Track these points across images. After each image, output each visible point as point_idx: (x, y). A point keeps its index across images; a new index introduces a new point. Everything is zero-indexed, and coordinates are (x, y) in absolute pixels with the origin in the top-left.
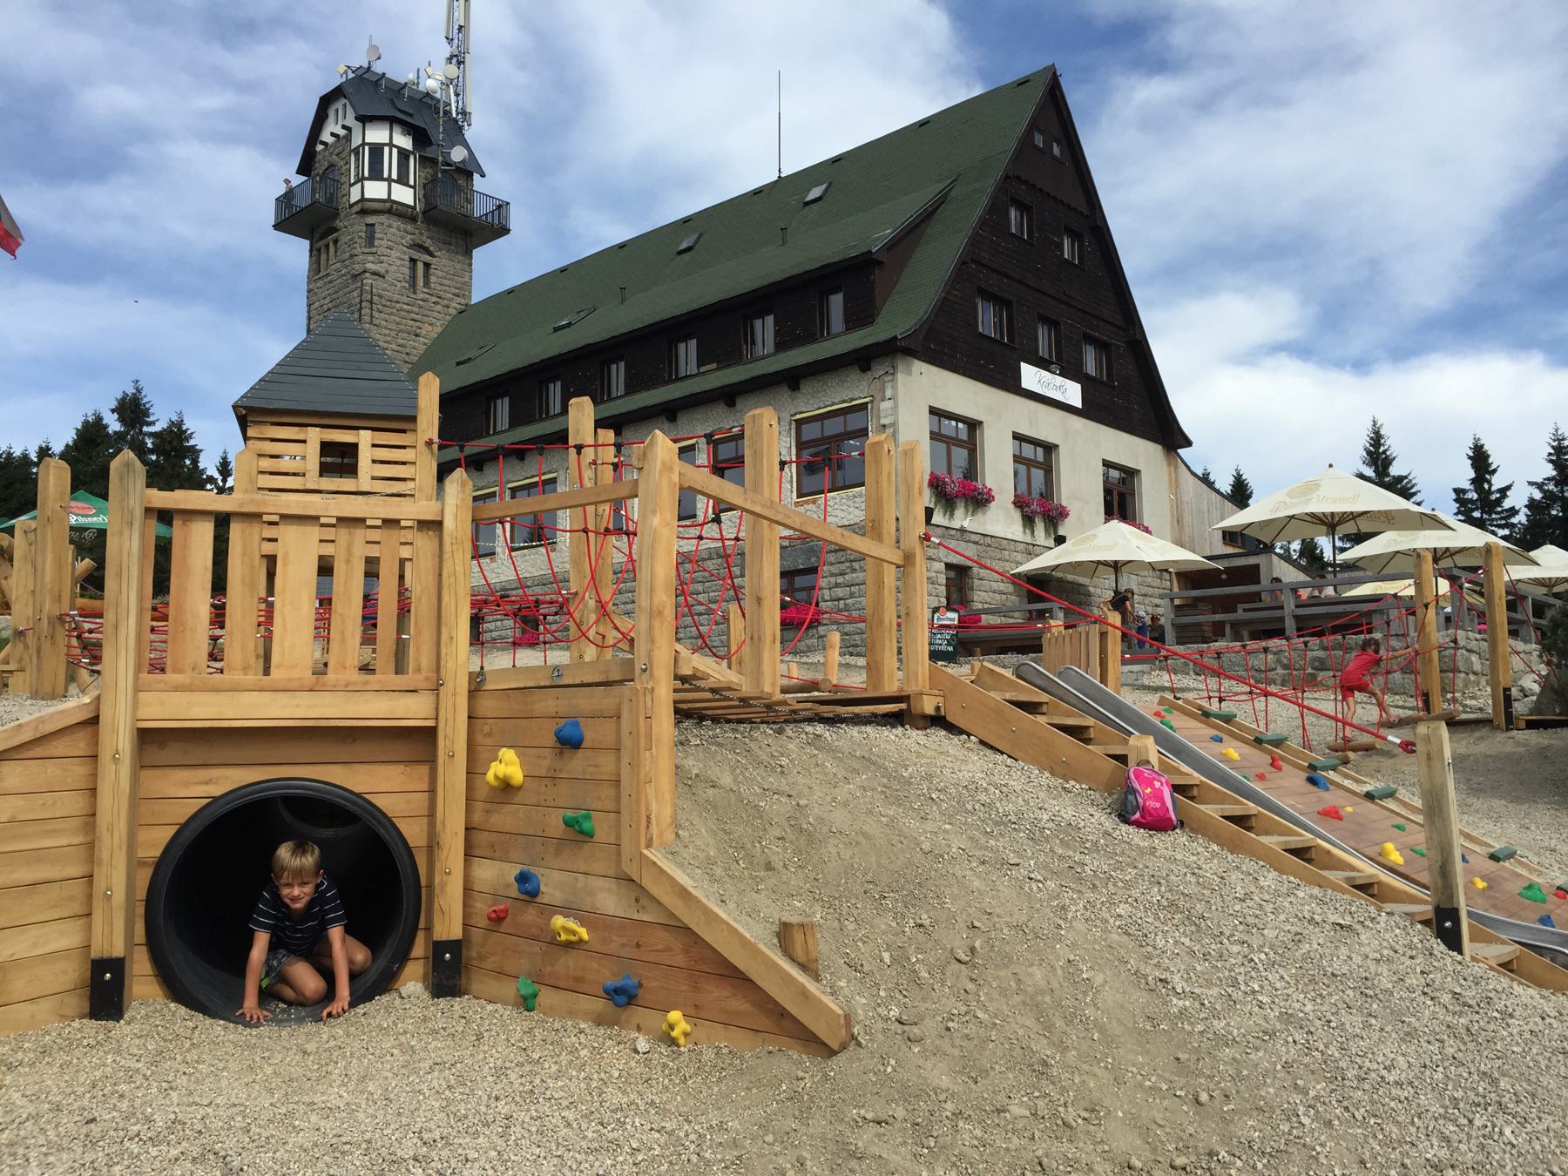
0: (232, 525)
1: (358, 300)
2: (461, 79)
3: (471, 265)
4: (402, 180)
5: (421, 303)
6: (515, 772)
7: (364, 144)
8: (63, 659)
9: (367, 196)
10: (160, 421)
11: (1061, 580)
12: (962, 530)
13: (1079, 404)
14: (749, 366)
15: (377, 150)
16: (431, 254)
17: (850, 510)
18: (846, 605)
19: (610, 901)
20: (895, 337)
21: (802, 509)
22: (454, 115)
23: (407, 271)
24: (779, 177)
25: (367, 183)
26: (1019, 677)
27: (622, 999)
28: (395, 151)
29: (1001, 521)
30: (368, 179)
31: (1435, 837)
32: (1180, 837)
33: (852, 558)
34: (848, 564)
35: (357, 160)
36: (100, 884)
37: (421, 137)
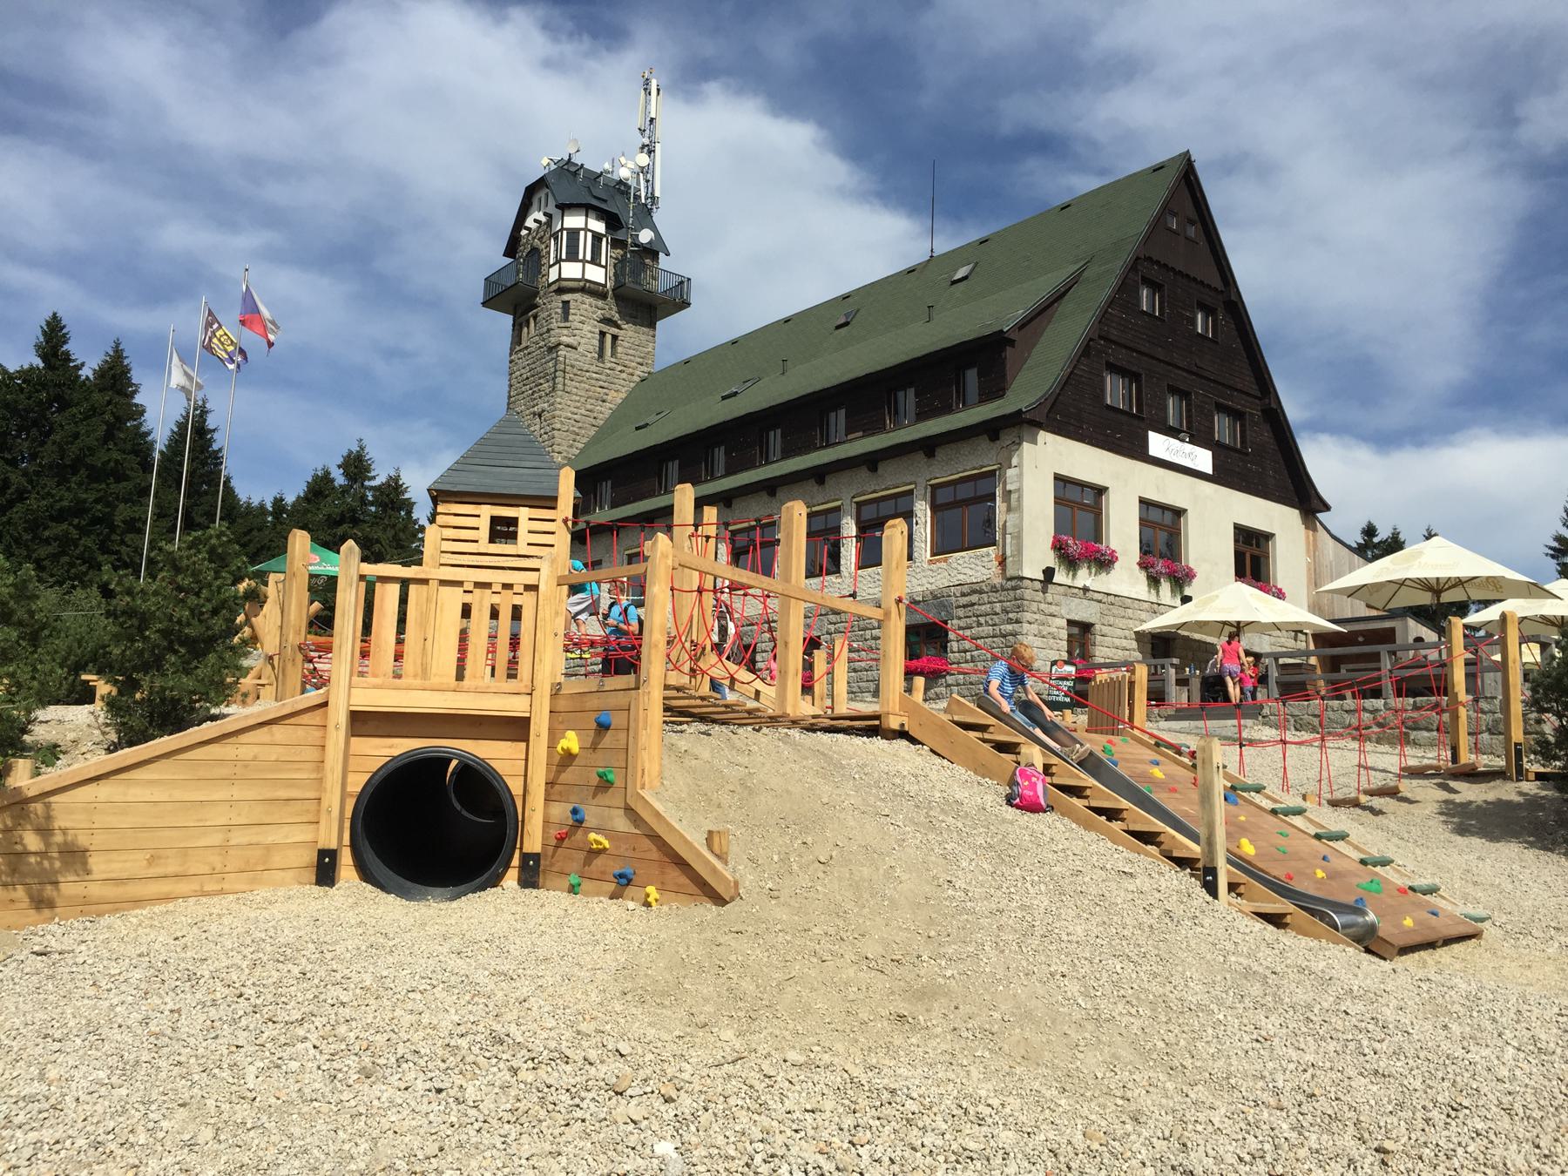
0: (411, 586)
1: (552, 370)
2: (651, 167)
3: (654, 336)
4: (595, 260)
5: (608, 371)
6: (575, 749)
7: (562, 229)
8: (300, 676)
9: (563, 276)
10: (380, 477)
11: (1187, 638)
12: (1085, 590)
13: (1209, 470)
14: (891, 434)
15: (574, 234)
16: (619, 327)
17: (978, 568)
18: (972, 656)
19: (622, 824)
20: (1021, 410)
21: (934, 567)
22: (643, 201)
23: (596, 343)
24: (932, 257)
25: (563, 264)
26: (979, 706)
27: (624, 881)
28: (589, 235)
29: (1127, 579)
30: (564, 261)
31: (1205, 817)
32: (1049, 817)
33: (978, 613)
34: (975, 619)
35: (556, 244)
36: (325, 804)
37: (613, 222)
